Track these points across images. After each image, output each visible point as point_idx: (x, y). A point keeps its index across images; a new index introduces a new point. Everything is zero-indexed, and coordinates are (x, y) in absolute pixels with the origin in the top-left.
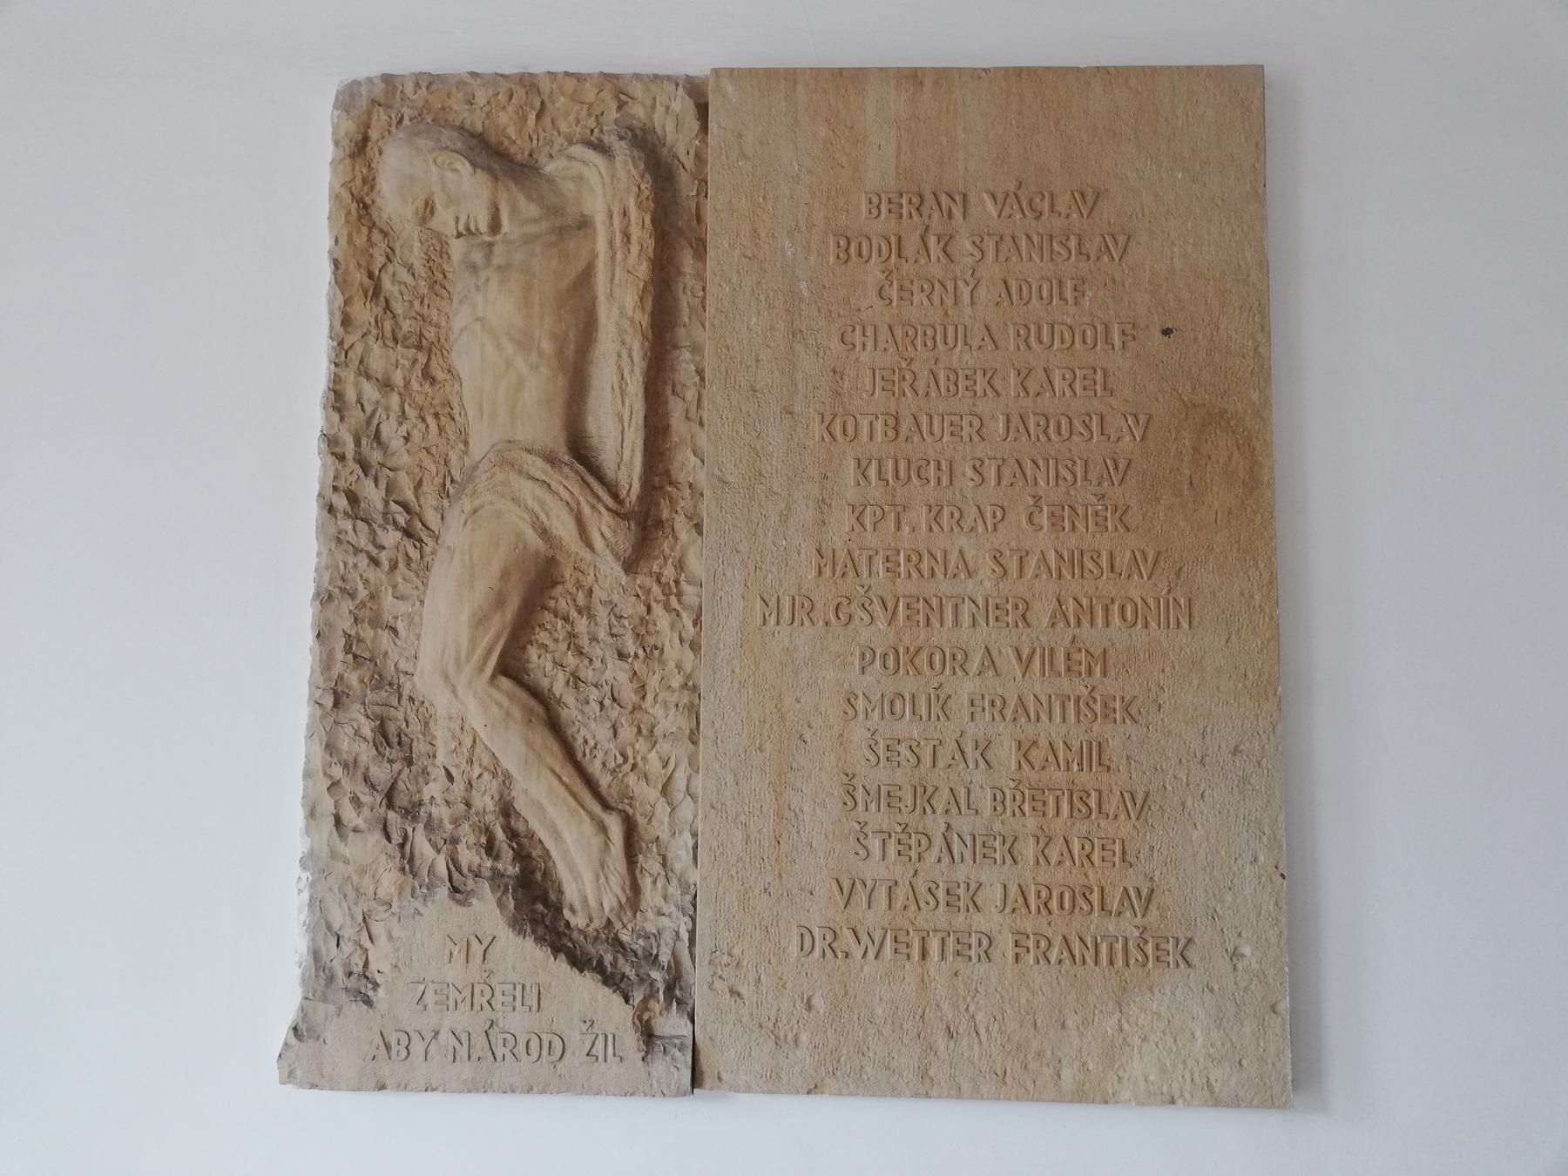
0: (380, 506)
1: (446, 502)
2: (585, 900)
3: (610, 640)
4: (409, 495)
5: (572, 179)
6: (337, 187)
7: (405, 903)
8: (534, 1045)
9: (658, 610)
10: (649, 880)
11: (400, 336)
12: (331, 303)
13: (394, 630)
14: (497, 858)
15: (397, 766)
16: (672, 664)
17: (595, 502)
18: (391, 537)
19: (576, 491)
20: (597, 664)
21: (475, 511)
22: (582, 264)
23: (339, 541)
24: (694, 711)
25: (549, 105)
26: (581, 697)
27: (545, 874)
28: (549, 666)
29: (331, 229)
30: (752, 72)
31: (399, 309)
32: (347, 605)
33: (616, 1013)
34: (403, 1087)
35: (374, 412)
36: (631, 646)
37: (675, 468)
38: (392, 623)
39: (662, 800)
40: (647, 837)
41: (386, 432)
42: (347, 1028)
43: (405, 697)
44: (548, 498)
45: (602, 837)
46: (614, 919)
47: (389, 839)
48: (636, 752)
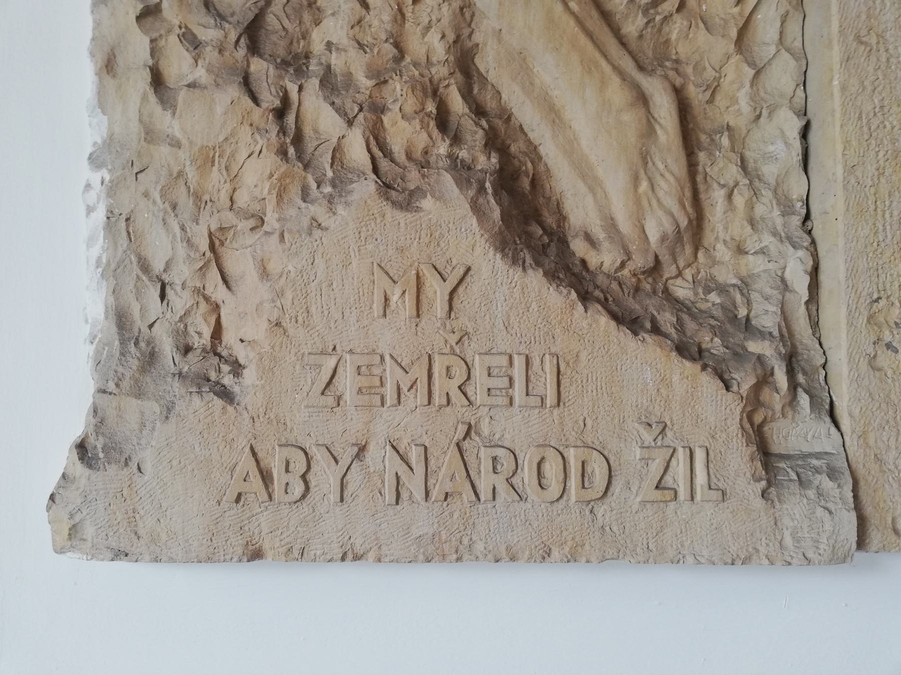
2: (611, 225)
7: (292, 212)
8: (552, 470)
10: (719, 195)
14: (456, 140)
27: (534, 182)
33: (711, 409)
34: (298, 554)
39: (735, 59)
40: (708, 126)
42: (182, 444)
45: (642, 112)
46: (665, 258)
47: (255, 100)
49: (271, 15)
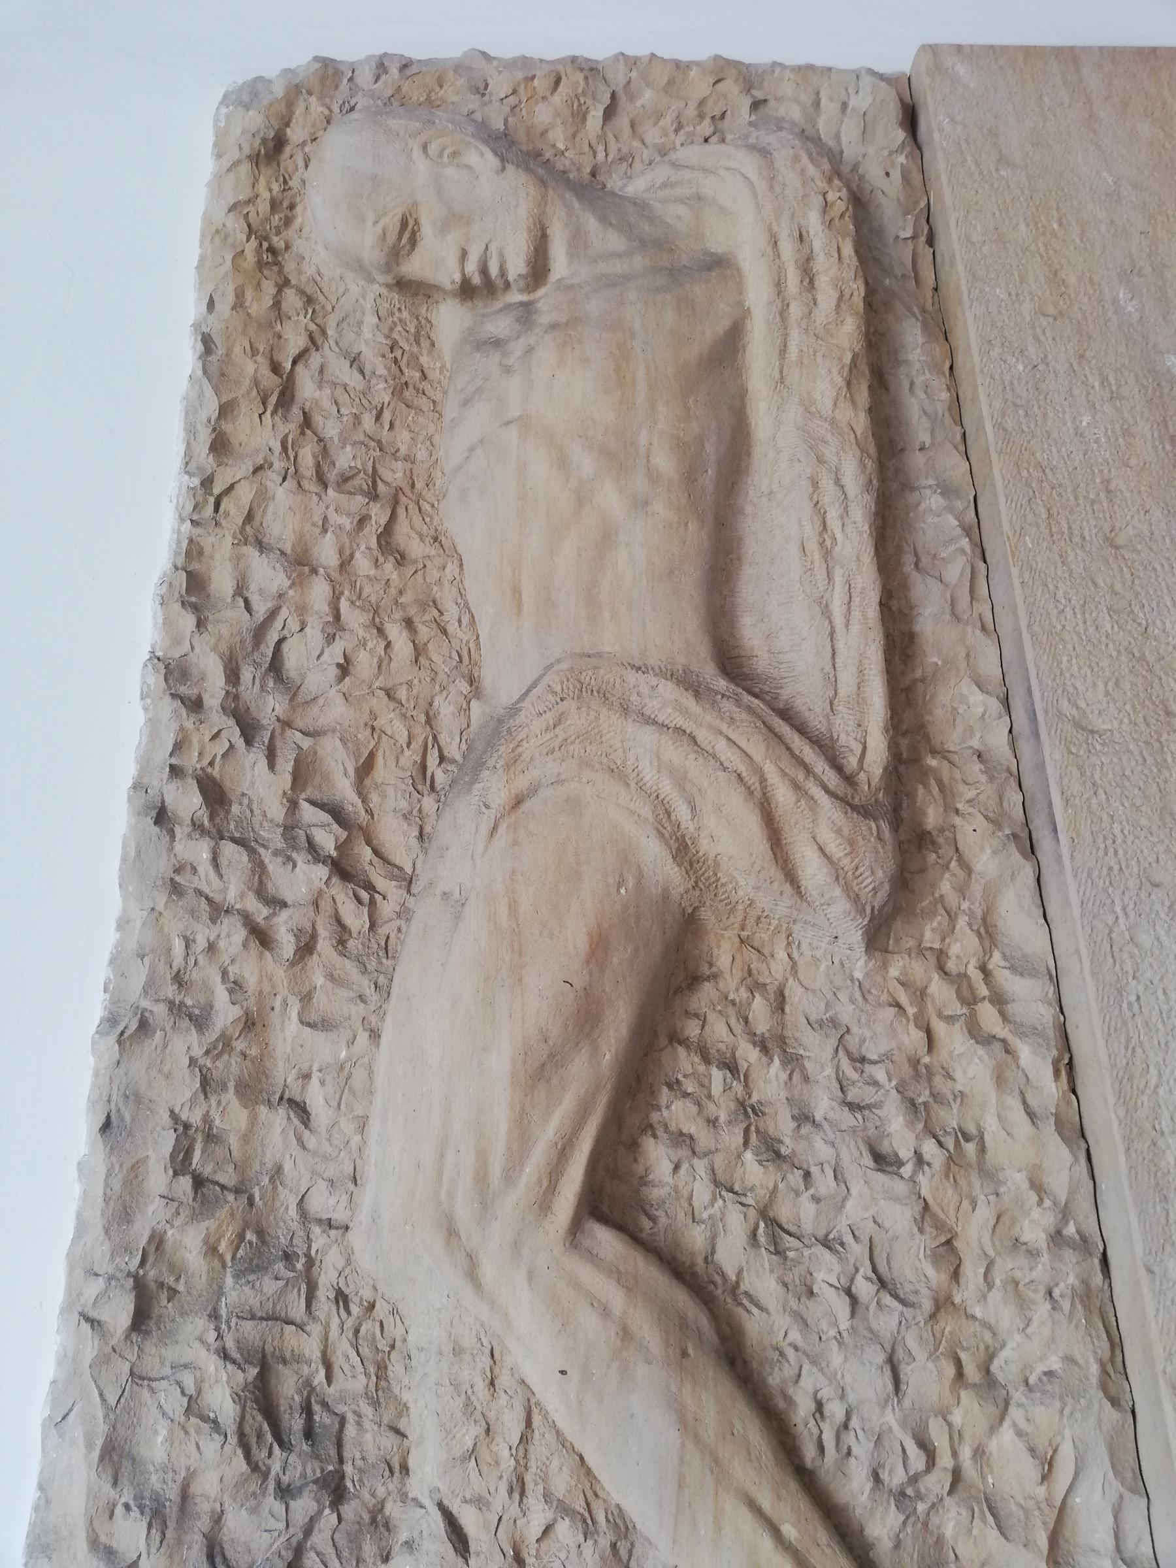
0: (277, 811)
1: (429, 803)
3: (847, 1119)
4: (344, 789)
5: (681, 200)
6: (220, 215)
9: (954, 1041)
11: (332, 477)
12: (189, 413)
13: (300, 1110)
15: (303, 1506)
16: (1016, 1180)
17: (800, 775)
18: (300, 880)
19: (757, 748)
20: (825, 1184)
21: (518, 802)
22: (723, 326)
23: (176, 889)
24: (1099, 1308)
25: (623, 99)
26: (794, 1276)
28: (702, 1191)
29: (201, 283)
30: (995, 51)
31: (331, 429)
32: (187, 1044)
35: (273, 614)
36: (900, 1135)
37: (938, 714)
38: (294, 1092)
41: (293, 660)
43: (324, 1293)
44: (693, 766)
48: (956, 1437)
49: (312, 1554)
